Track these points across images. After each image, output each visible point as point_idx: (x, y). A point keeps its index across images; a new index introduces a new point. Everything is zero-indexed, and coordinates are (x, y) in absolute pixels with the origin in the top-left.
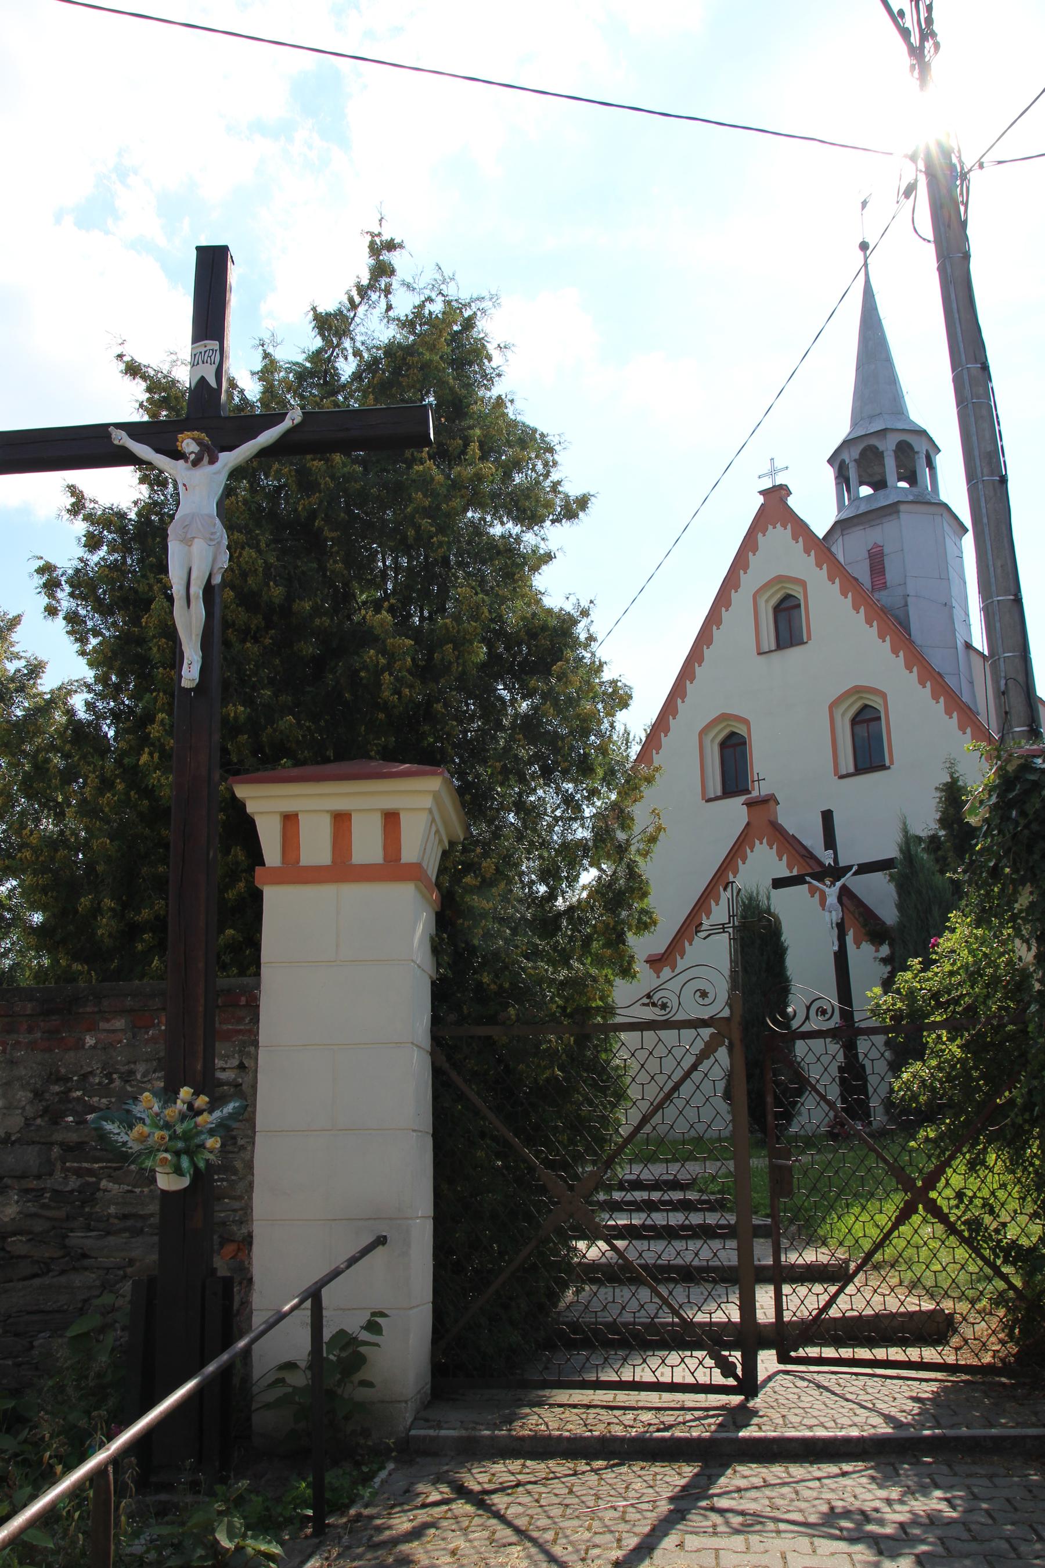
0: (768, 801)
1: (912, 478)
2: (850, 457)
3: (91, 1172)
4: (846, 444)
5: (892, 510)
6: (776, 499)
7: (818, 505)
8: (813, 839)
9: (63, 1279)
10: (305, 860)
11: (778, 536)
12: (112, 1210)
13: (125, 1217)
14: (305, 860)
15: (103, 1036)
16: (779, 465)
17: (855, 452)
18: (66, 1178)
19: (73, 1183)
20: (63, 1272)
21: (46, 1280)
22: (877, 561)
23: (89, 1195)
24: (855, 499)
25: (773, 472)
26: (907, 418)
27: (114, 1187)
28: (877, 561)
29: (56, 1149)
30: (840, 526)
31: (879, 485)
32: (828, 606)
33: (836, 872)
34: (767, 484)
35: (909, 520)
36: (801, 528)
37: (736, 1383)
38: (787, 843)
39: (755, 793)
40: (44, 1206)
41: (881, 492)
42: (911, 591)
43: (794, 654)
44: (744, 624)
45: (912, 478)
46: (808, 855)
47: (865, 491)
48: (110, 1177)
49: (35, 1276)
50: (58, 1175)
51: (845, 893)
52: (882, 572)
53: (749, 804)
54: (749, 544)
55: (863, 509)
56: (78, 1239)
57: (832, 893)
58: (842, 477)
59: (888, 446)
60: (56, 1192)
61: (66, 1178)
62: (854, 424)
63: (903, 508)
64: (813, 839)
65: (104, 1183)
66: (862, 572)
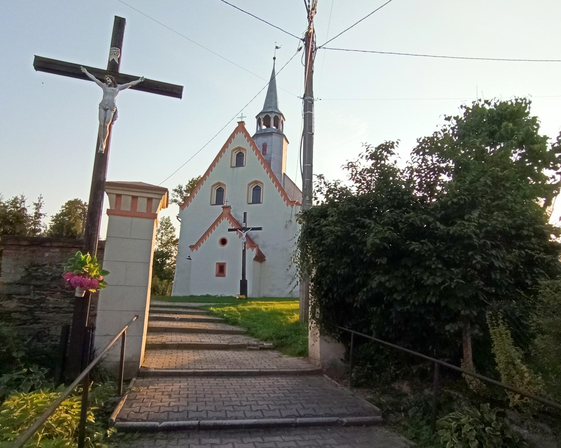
0: (229, 207)
1: (277, 126)
2: (262, 117)
3: (43, 294)
4: (261, 113)
5: (271, 134)
6: (241, 124)
7: (252, 129)
8: (241, 220)
9: (31, 326)
10: (122, 209)
11: (240, 135)
12: (50, 305)
13: (55, 308)
14: (122, 209)
15: (51, 254)
16: (244, 115)
17: (263, 116)
18: (35, 295)
19: (37, 297)
20: (31, 324)
21: (25, 326)
22: (265, 146)
23: (43, 301)
24: (261, 129)
25: (242, 117)
26: (276, 107)
27: (51, 299)
28: (265, 146)
29: (32, 287)
30: (256, 136)
31: (268, 126)
32: (250, 156)
33: (246, 229)
34: (240, 120)
35: (275, 138)
36: (247, 134)
37: (548, 150)
38: (232, 219)
39: (225, 205)
40: (26, 304)
41: (269, 129)
42: (272, 157)
43: (241, 168)
44: (230, 158)
45: (277, 126)
46: (237, 223)
47: (264, 127)
48: (50, 296)
49: (20, 325)
50: (32, 294)
51: (247, 236)
52: (266, 150)
53: (223, 207)
54: (232, 136)
55: (263, 132)
56: (37, 313)
57: (244, 235)
58: (259, 123)
59: (272, 116)
60: (30, 299)
61: (35, 295)
62: (264, 108)
63: (274, 134)
64: (241, 220)
65: (48, 298)
66: (260, 149)
